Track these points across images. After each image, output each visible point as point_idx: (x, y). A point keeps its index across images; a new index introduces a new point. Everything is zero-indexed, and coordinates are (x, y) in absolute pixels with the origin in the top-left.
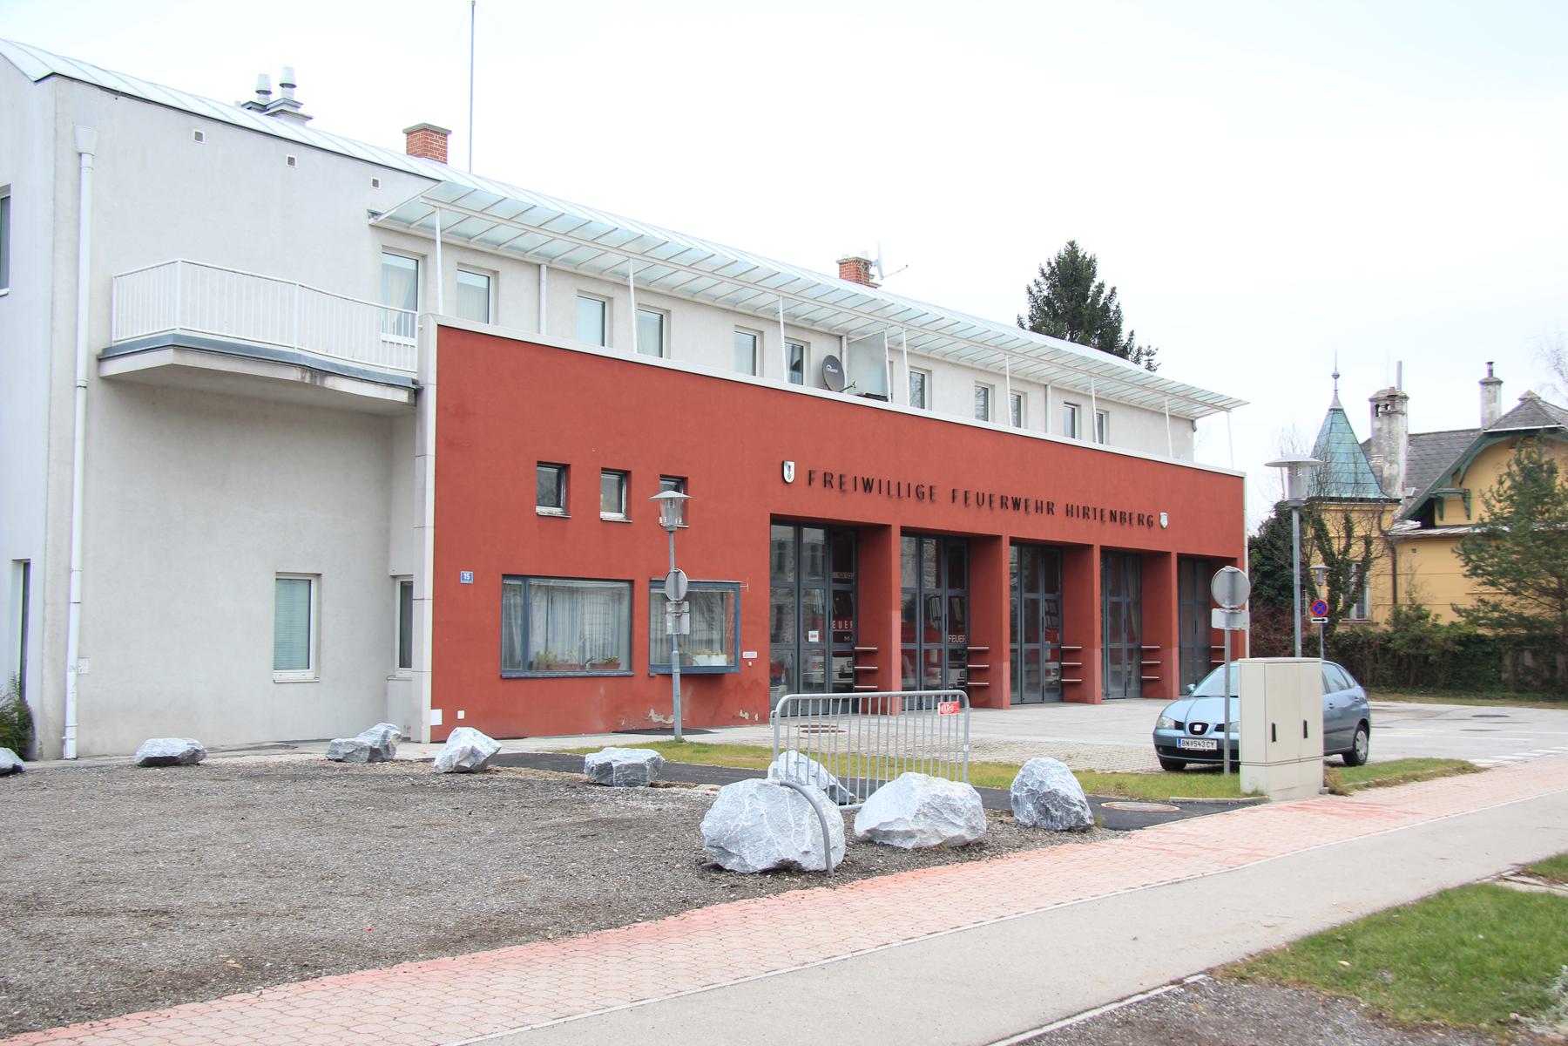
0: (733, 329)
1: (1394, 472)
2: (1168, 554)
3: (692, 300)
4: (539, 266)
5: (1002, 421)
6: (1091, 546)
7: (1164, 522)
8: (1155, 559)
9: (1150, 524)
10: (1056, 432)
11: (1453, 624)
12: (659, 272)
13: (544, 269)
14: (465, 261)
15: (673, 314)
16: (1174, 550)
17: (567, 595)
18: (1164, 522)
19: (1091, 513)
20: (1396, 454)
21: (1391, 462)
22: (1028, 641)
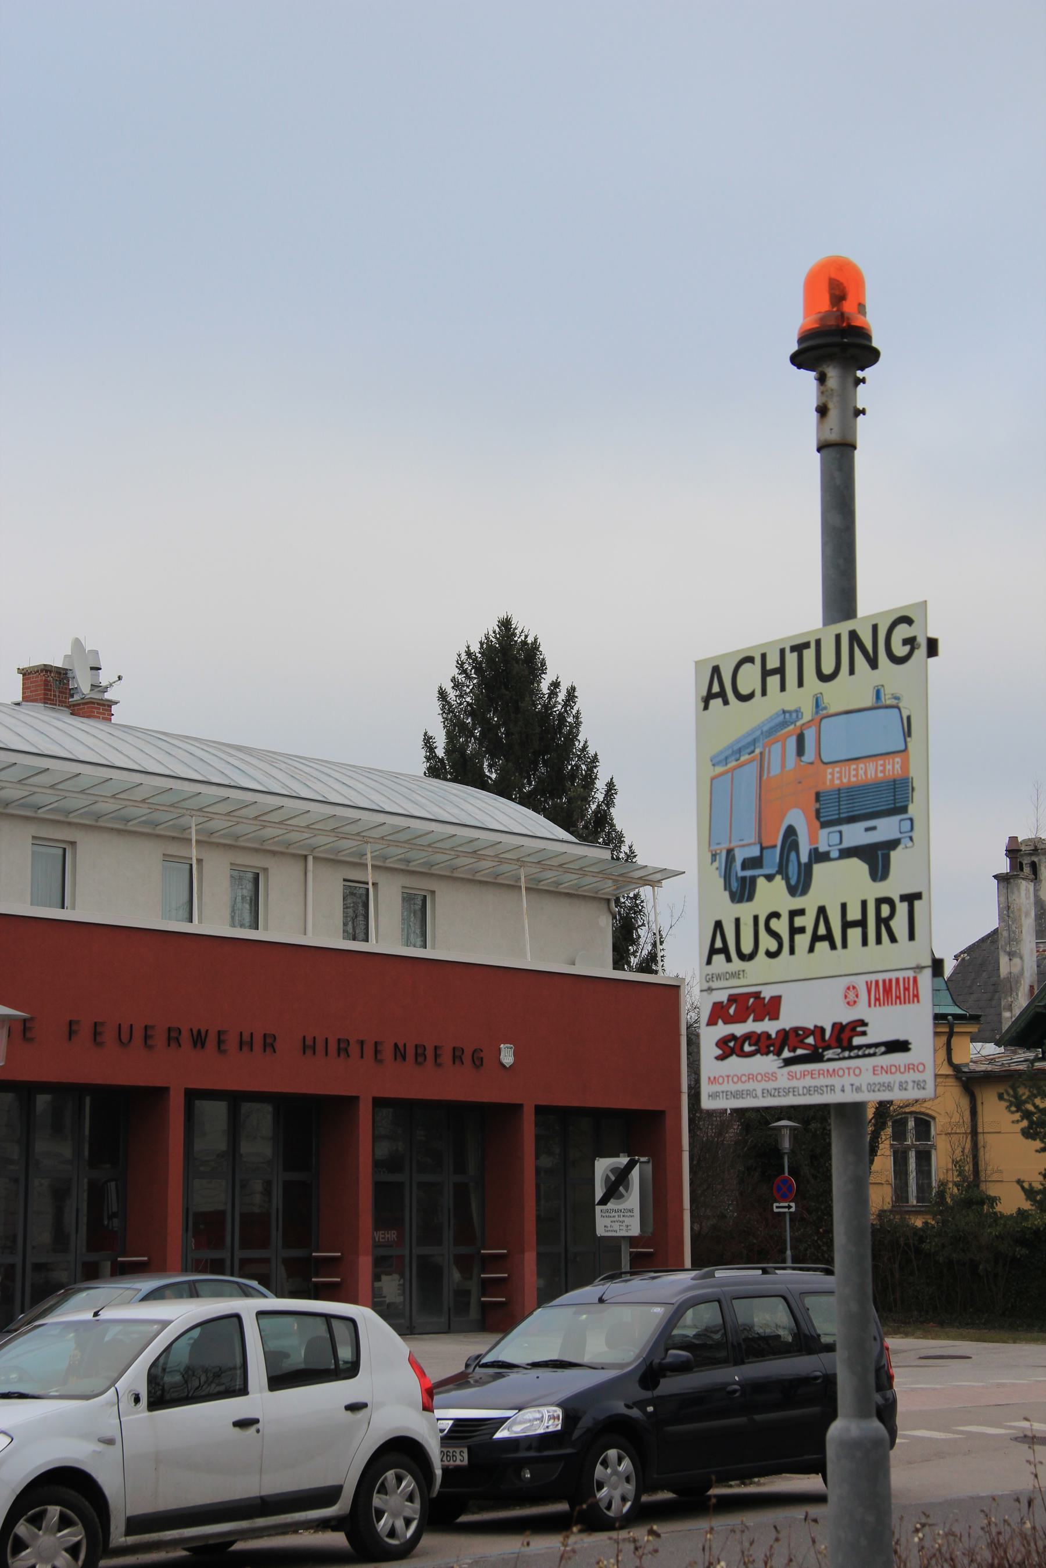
0: (30, 841)
1: (1016, 970)
2: (515, 1109)
3: (96, 825)
4: (305, 857)
5: (387, 937)
6: (355, 1099)
7: (507, 1057)
8: (493, 1119)
9: (478, 1061)
10: (325, 932)
11: (1020, 1212)
12: (217, 824)
13: (310, 859)
14: (239, 861)
15: (271, 871)
16: (529, 1097)
17: (980, 1137)
18: (507, 1057)
19: (354, 1049)
20: (1018, 941)
21: (1011, 955)
22: (245, 1244)
